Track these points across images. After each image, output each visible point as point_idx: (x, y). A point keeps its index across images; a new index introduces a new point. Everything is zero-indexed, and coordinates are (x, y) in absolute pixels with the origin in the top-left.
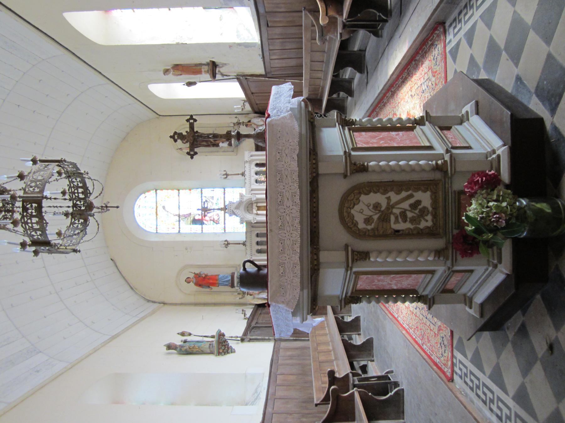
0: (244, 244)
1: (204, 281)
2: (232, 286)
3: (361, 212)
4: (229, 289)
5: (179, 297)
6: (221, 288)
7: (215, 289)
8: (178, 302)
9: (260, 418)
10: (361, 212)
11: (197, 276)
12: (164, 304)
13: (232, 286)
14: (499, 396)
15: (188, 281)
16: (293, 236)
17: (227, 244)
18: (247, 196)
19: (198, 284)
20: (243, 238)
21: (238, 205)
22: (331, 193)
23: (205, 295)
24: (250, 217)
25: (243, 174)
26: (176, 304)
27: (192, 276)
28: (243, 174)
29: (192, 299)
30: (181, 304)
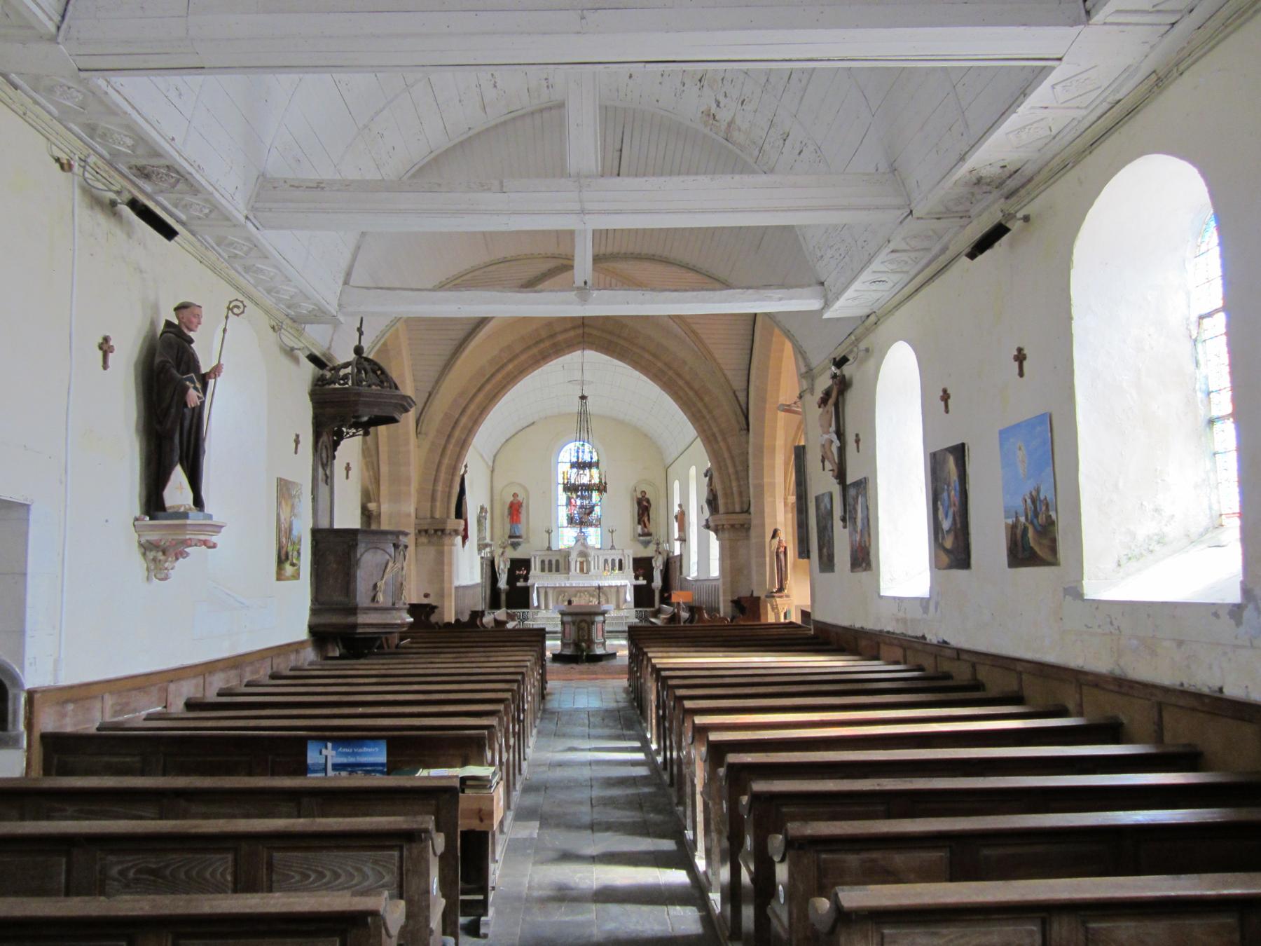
0: (549, 548)
1: (515, 509)
2: (510, 537)
3: (584, 625)
4: (507, 533)
5: (498, 486)
6: (508, 526)
7: (507, 520)
8: (495, 484)
9: (6, 496)
10: (584, 625)
11: (520, 505)
12: (492, 471)
13: (510, 537)
14: (1054, 73)
15: (515, 495)
16: (578, 610)
17: (549, 532)
18: (592, 553)
19: (512, 505)
20: (554, 548)
21: (585, 545)
22: (587, 618)
23: (501, 510)
24: (574, 556)
25: (613, 548)
26: (492, 482)
27: (520, 498)
28: (613, 548)
29: (496, 497)
30: (492, 487)
